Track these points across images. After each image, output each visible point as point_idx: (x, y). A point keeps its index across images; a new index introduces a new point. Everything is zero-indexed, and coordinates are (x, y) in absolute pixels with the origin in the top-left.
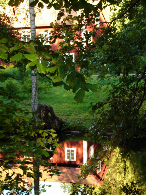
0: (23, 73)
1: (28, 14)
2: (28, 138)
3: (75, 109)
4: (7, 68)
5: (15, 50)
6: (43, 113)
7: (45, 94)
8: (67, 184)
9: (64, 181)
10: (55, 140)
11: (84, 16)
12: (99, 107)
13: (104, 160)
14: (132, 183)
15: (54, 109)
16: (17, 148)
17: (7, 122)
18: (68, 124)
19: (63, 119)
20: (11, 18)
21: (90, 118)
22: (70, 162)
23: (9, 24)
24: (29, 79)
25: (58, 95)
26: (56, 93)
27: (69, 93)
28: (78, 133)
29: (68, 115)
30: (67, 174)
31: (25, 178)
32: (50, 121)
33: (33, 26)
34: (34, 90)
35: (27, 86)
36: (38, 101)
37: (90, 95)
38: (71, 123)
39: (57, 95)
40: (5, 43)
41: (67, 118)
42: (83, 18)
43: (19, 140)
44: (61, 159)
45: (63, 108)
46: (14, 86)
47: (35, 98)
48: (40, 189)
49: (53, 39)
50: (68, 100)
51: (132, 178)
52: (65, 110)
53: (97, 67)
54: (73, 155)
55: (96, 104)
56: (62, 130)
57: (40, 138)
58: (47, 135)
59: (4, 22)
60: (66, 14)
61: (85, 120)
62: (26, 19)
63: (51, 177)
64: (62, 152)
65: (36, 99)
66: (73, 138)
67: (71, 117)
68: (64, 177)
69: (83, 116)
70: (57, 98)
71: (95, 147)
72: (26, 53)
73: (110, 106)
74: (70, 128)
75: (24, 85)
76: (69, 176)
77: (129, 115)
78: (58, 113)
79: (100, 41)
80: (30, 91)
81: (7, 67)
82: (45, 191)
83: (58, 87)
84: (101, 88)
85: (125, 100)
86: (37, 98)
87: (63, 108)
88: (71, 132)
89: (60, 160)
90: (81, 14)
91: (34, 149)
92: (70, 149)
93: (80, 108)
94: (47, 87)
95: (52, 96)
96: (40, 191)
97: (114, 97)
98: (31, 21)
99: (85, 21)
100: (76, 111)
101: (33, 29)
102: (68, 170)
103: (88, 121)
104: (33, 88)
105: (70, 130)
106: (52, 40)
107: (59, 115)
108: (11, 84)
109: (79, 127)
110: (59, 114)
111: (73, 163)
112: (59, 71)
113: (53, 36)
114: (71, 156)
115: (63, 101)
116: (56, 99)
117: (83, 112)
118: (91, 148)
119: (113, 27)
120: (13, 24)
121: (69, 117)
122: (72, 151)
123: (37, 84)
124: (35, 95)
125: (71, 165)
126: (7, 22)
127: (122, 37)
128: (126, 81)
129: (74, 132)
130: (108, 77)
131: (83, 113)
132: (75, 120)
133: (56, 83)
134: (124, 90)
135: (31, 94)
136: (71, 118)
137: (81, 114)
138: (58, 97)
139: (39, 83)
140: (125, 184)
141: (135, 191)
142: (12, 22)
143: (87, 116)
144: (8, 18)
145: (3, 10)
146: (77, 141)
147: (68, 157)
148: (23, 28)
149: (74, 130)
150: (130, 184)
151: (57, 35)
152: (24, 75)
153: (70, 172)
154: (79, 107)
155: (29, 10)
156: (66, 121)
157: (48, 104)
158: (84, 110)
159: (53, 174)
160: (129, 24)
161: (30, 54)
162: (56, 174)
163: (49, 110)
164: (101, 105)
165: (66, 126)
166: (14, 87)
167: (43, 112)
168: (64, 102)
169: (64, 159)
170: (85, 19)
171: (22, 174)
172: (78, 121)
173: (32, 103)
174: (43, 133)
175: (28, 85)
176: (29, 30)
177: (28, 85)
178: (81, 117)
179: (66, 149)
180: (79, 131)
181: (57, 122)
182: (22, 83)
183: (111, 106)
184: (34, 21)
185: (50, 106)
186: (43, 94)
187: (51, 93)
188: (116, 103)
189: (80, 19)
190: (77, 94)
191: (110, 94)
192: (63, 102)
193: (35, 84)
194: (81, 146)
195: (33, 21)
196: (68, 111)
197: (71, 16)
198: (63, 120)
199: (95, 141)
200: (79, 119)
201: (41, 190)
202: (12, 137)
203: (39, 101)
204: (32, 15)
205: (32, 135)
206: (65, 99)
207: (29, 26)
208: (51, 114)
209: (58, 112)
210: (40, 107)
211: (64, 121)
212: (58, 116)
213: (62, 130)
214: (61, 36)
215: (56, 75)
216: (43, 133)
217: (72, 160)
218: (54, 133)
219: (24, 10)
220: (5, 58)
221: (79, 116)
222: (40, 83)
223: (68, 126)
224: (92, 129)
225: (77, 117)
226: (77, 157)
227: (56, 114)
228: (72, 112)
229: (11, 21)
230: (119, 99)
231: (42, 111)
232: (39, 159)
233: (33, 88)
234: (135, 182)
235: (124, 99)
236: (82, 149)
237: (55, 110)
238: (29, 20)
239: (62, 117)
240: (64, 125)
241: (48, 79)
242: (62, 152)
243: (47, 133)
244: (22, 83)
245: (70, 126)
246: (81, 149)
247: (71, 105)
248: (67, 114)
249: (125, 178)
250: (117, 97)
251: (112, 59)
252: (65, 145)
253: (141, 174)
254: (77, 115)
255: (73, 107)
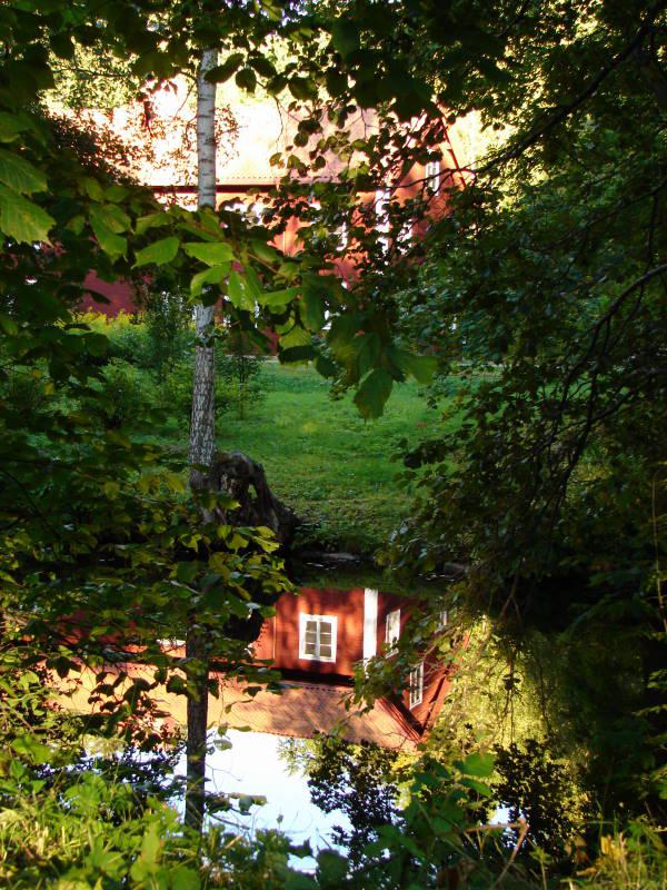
0: (164, 346)
1: (193, 137)
2: (181, 554)
3: (341, 475)
4: (110, 326)
5: (153, 225)
6: (229, 486)
7: (237, 419)
8: (301, 742)
9: (292, 732)
10: (270, 564)
11: (389, 139)
12: (430, 460)
13: (437, 648)
14: (531, 744)
15: (267, 474)
16: (136, 591)
17: (107, 492)
18: (315, 526)
19: (300, 508)
20: (131, 150)
21: (393, 511)
22: (316, 664)
23: (123, 169)
24: (185, 367)
25: (284, 427)
26: (277, 419)
27: (324, 422)
28: (348, 560)
29: (316, 499)
30: (303, 705)
31: (159, 694)
32: (252, 514)
33: (207, 181)
34: (200, 400)
35: (177, 389)
36: (214, 442)
37: (397, 432)
38: (325, 527)
39: (278, 427)
40: (118, 201)
41: (312, 508)
42: (386, 147)
43: (147, 558)
44: (285, 654)
45: (301, 471)
46: (130, 387)
47: (205, 432)
48: (209, 740)
49: (276, 219)
50: (317, 444)
51: (529, 730)
52: (308, 478)
53: (427, 331)
54: (326, 639)
55: (421, 447)
56: (293, 547)
57: (222, 553)
58: (245, 544)
59: (107, 160)
60: (330, 129)
61: (373, 517)
62: (185, 153)
63: (251, 698)
64: (290, 629)
65: (207, 435)
66: (329, 576)
67: (326, 502)
68: (291, 717)
69: (368, 502)
70: (281, 436)
71: (406, 617)
72: (188, 237)
73: (470, 455)
74: (322, 542)
75: (166, 386)
76: (309, 712)
77: (532, 494)
78: (283, 487)
79: (440, 237)
80: (188, 408)
81: (107, 323)
82: (226, 746)
83: (296, 366)
84: (437, 404)
85: (522, 439)
86: (209, 429)
87: (301, 471)
88: (325, 555)
89: (282, 658)
90: (381, 130)
91: (194, 595)
92: (316, 618)
93: (360, 475)
94: (246, 398)
95: (265, 427)
96: (209, 747)
97: (482, 424)
98: (201, 161)
99: (391, 158)
100: (346, 485)
101: (206, 188)
102: (308, 692)
103: (385, 519)
104: (199, 397)
105: (322, 549)
106: (273, 224)
107: (286, 495)
108: (119, 379)
109: (354, 538)
110: (285, 490)
111: (326, 670)
112: (303, 304)
113: (277, 209)
114: (319, 645)
115: (303, 421)
116: (275, 441)
117: (370, 488)
118: (392, 619)
119: (488, 189)
120: (139, 169)
121: (320, 503)
122: (325, 627)
123: (212, 384)
124: (204, 422)
125: (318, 676)
126: (117, 161)
127: (520, 224)
128: (525, 378)
129: (332, 555)
130: (463, 368)
131: (367, 491)
132: (339, 515)
133: (290, 350)
134: (521, 402)
135: (189, 419)
136: (326, 506)
137: (360, 496)
138: (282, 431)
139: (221, 381)
140: (506, 747)
141: (541, 772)
142: (136, 163)
143: (384, 503)
144: (120, 149)
145: (107, 120)
146: (345, 589)
147: (310, 649)
148: (154, 240)
149: (337, 551)
150: (522, 749)
151: (292, 206)
152: (167, 353)
153: (314, 701)
154: (357, 470)
155: (194, 122)
156: (309, 516)
157: (250, 455)
158: (372, 483)
159: (259, 689)
160: (545, 187)
161: (206, 242)
162: (268, 688)
163: (249, 475)
164: (435, 451)
165: (306, 534)
166: (130, 391)
167: (228, 480)
168: (304, 452)
169: (295, 651)
170: (393, 150)
171: (151, 681)
172: (351, 518)
173: (192, 447)
174: (230, 537)
175: (181, 386)
176: (192, 196)
177: (181, 386)
178: (360, 507)
179: (304, 618)
180: (353, 554)
181: (276, 519)
182: (161, 380)
183: (473, 457)
184: (212, 161)
185: (253, 462)
186: (231, 420)
187: (259, 419)
188: (489, 449)
189: (375, 149)
190: (363, 387)
191: (470, 415)
192: (300, 451)
193: (206, 383)
194: (356, 609)
195: (208, 162)
196: (316, 483)
197: (347, 134)
198: (298, 513)
199: (388, 694)
200: (354, 511)
201: (215, 742)
202: (123, 547)
203: (217, 441)
204: (204, 140)
205: (194, 544)
206: (309, 442)
207: (194, 181)
208: (258, 492)
209: (282, 484)
210: (221, 465)
211: (303, 518)
212: (281, 500)
213: (293, 547)
214: (304, 209)
215: (291, 322)
216: (230, 537)
217: (324, 659)
218: (272, 539)
219: (179, 123)
220: (120, 252)
221: (356, 502)
222: (223, 379)
223: (315, 536)
224: (400, 538)
225: (348, 504)
226: (339, 648)
227: (274, 492)
228: (332, 487)
229: (129, 158)
230: (499, 433)
231: (225, 478)
232: (213, 632)
233: (199, 397)
234: (541, 740)
235: (516, 436)
236: (359, 622)
237: (270, 477)
238: (194, 158)
239: (294, 501)
240: (300, 531)
241: (259, 340)
242: (290, 629)
243: (244, 537)
244: (161, 380)
245: (321, 536)
246: (355, 622)
247: (329, 464)
248: (312, 492)
249: (509, 715)
250: (493, 426)
251: (480, 297)
252: (302, 605)
253: (565, 716)
254: (347, 498)
255: (336, 470)
